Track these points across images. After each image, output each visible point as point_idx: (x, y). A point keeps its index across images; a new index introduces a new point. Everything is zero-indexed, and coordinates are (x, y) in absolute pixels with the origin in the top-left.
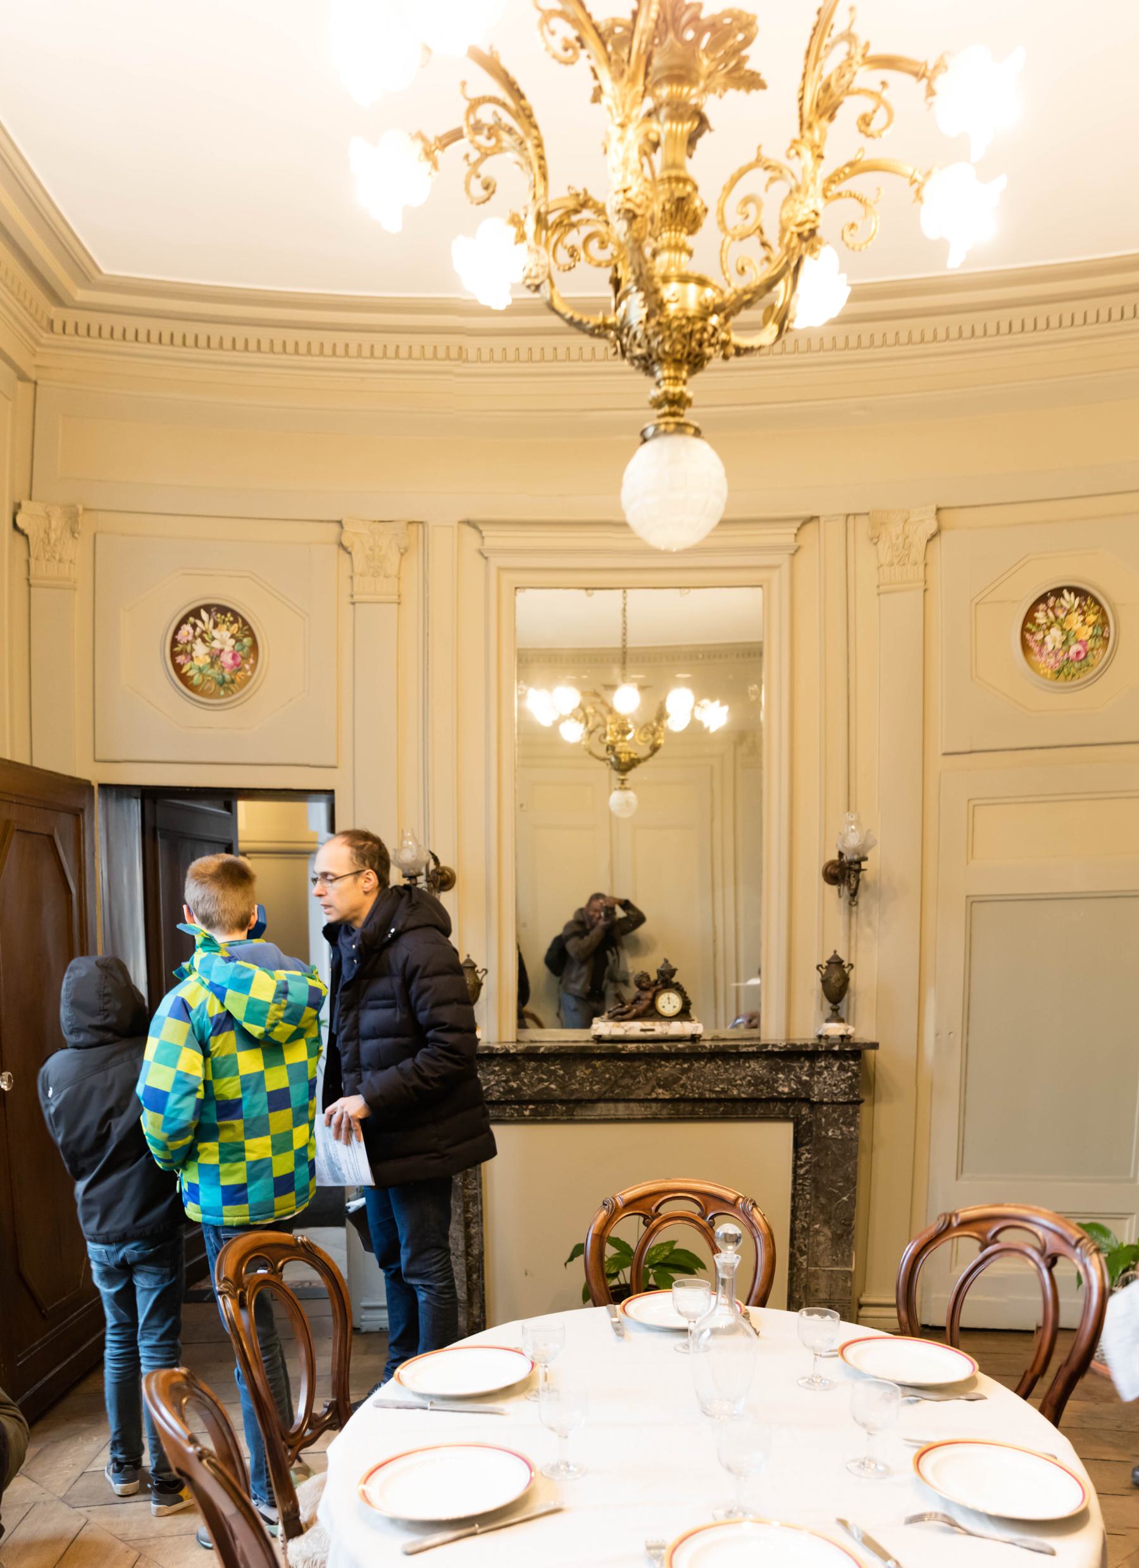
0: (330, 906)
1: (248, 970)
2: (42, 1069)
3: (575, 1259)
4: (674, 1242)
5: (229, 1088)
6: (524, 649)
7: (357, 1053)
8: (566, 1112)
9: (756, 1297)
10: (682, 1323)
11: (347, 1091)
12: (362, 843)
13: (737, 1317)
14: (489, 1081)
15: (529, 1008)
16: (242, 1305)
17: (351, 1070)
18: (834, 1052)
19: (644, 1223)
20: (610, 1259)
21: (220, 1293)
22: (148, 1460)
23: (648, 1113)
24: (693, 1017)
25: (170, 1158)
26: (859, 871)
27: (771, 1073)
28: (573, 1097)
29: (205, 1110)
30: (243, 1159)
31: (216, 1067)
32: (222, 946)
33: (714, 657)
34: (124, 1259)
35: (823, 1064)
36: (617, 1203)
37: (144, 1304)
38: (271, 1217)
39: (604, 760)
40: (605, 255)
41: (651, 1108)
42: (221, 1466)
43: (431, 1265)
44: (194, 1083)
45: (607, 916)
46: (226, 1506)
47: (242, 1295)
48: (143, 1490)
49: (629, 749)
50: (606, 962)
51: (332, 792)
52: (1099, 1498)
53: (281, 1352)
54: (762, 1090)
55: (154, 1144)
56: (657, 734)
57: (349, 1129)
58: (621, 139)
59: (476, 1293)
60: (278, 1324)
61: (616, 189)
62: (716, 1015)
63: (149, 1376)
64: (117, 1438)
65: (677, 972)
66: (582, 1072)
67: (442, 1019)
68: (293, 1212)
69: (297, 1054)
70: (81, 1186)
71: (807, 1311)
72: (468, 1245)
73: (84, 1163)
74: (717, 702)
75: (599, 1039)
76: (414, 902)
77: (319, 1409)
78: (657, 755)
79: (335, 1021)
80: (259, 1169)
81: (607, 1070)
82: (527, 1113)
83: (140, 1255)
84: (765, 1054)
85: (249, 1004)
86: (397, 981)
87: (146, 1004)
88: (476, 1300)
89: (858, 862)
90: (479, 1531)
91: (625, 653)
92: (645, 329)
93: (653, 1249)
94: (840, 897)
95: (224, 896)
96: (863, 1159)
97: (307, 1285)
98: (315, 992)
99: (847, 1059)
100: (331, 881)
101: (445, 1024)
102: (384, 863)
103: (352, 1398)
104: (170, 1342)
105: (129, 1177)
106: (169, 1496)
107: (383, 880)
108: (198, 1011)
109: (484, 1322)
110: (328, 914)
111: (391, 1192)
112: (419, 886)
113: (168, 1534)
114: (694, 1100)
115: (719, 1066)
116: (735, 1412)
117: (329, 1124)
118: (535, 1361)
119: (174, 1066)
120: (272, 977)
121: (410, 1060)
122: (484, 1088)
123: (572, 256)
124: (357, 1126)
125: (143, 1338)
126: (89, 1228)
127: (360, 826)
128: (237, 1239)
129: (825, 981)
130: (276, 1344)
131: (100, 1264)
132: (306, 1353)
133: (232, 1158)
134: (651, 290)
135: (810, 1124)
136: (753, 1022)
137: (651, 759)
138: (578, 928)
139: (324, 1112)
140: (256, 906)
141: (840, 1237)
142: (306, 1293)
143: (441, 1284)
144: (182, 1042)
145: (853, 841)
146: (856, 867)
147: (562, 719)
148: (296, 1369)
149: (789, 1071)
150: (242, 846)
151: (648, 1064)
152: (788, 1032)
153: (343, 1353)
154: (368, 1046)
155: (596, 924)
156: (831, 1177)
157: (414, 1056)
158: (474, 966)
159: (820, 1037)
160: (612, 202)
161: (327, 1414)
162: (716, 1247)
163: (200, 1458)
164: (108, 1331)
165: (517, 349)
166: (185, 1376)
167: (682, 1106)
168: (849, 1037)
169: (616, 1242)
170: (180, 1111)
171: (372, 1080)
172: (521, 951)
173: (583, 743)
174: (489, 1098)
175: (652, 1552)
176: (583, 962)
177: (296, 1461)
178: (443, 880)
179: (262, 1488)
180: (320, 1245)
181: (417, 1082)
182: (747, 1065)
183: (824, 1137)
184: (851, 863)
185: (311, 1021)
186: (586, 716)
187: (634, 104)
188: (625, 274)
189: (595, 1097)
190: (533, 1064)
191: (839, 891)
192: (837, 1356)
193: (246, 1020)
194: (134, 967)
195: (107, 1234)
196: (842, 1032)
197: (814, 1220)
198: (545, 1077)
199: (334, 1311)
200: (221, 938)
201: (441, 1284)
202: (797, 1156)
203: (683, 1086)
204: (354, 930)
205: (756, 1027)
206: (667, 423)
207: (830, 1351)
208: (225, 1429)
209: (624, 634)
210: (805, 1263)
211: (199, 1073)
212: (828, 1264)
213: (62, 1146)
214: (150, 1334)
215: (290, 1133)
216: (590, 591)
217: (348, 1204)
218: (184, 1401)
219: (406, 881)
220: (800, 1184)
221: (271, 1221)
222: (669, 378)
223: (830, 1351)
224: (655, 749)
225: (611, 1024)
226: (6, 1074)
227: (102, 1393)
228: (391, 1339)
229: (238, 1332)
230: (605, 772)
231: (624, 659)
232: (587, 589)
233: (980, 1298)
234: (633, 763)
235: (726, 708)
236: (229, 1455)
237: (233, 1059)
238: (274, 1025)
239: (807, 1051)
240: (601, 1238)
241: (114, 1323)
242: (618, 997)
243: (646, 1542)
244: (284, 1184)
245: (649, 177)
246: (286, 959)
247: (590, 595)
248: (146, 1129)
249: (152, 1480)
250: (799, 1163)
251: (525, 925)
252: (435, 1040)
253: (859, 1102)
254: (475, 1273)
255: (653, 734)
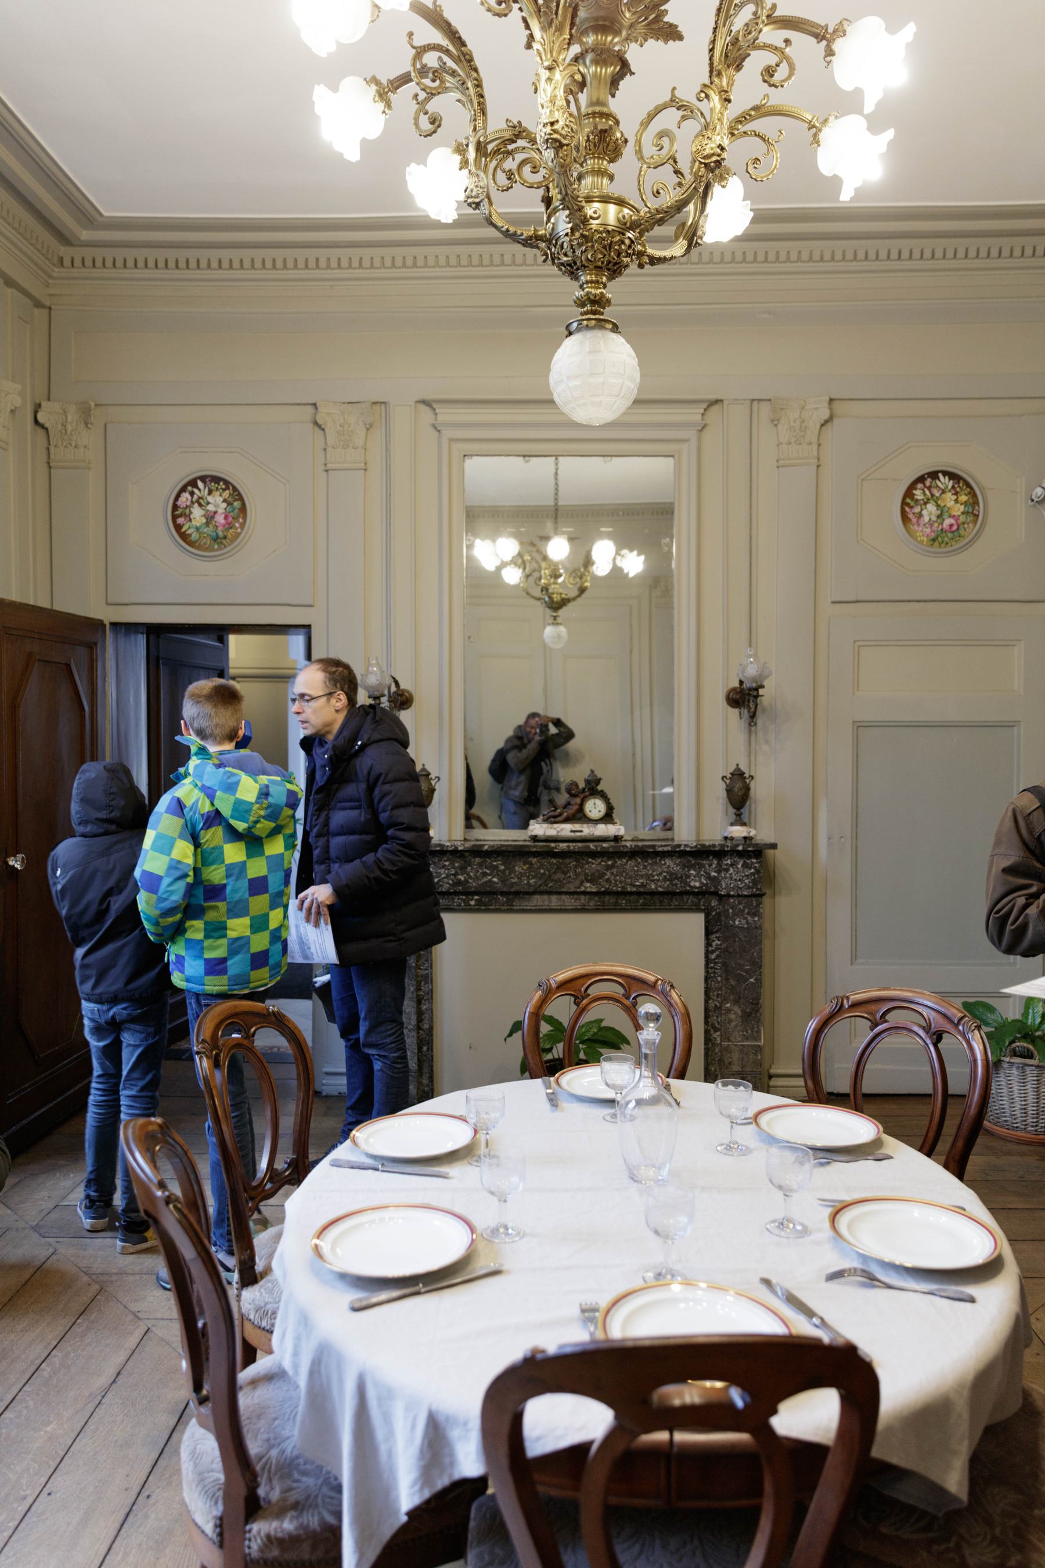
0: (306, 722)
1: (235, 775)
2: (53, 853)
3: (514, 1035)
4: (601, 1020)
5: (215, 875)
6: (471, 507)
7: (327, 848)
8: (507, 902)
9: (676, 1070)
10: (610, 1094)
11: (318, 880)
12: (334, 669)
13: (659, 1089)
14: (440, 874)
15: (474, 811)
16: (216, 1064)
17: (321, 862)
18: (738, 851)
19: (575, 1002)
20: (544, 1036)
21: (198, 1053)
22: (118, 1200)
23: (577, 904)
24: (616, 820)
25: (161, 932)
26: (757, 696)
27: (684, 869)
28: (513, 890)
29: (193, 892)
30: (225, 936)
31: (205, 856)
32: (213, 755)
33: (633, 514)
34: (113, 1017)
35: (729, 862)
36: (550, 985)
37: (129, 1058)
38: (247, 988)
39: (539, 599)
40: (538, 178)
41: (580, 900)
42: (186, 1211)
43: (386, 1037)
44: (186, 870)
45: (542, 731)
46: (187, 1251)
47: (217, 1055)
48: (111, 1228)
49: (561, 590)
50: (541, 773)
51: (309, 626)
52: (1011, 1245)
53: (249, 1109)
54: (676, 885)
55: (147, 920)
56: (584, 578)
57: (318, 913)
58: (549, 79)
59: (426, 1064)
60: (248, 1084)
61: (545, 122)
62: (635, 819)
63: (128, 1123)
64: (92, 1177)
65: (602, 782)
66: (520, 868)
67: (400, 820)
68: (266, 985)
69: (276, 847)
70: (80, 952)
71: (723, 1082)
72: (420, 1020)
73: (83, 933)
74: (635, 553)
75: (535, 838)
76: (377, 719)
77: (280, 1165)
78: (583, 596)
79: (309, 820)
80: (238, 945)
81: (542, 866)
82: (472, 903)
83: (128, 1014)
84: (679, 853)
85: (235, 803)
86: (363, 786)
87: (147, 802)
88: (425, 1070)
89: (757, 689)
90: (423, 1290)
91: (557, 510)
92: (571, 240)
93: (583, 1026)
94: (741, 718)
95: (216, 713)
96: (766, 945)
97: (276, 1050)
98: (292, 794)
99: (749, 857)
100: (308, 701)
101: (403, 824)
102: (352, 686)
103: (310, 1156)
104: (150, 1094)
105: (124, 947)
106: (135, 1236)
107: (352, 700)
108: (191, 809)
109: (432, 1090)
110: (304, 728)
111: (353, 970)
112: (382, 705)
113: (130, 1271)
114: (617, 894)
115: (639, 864)
116: (660, 1178)
117: (301, 908)
118: (478, 1128)
119: (169, 855)
120: (256, 782)
121: (373, 854)
122: (436, 880)
123: (509, 179)
124: (325, 910)
125: (125, 1089)
126: (85, 988)
127: (333, 655)
128: (215, 1006)
129: (729, 791)
130: (244, 1102)
131: (92, 1020)
132: (272, 1112)
133: (216, 934)
134: (576, 207)
135: (719, 914)
136: (668, 824)
137: (579, 599)
138: (517, 742)
139: (297, 898)
140: (243, 722)
141: (749, 1014)
142: (275, 1057)
143: (395, 1055)
144: (176, 835)
145: (752, 671)
146: (755, 693)
147: (504, 565)
148: (262, 1126)
149: (699, 868)
150: (232, 672)
151: (577, 861)
152: (698, 833)
153: (305, 1114)
154: (337, 842)
155: (533, 739)
156: (739, 961)
157: (376, 851)
158: (429, 774)
159: (726, 838)
160: (541, 133)
161: (287, 1170)
162: (639, 1024)
163: (167, 1203)
164: (94, 1080)
165: (470, 256)
166: (160, 1126)
167: (607, 898)
168: (751, 838)
169: (550, 1020)
170: (172, 892)
171: (340, 871)
172: (469, 761)
173: (522, 585)
174: (440, 889)
175: (587, 1314)
176: (522, 772)
177: (256, 1212)
178: (403, 700)
179: (222, 1236)
180: (290, 1015)
181: (378, 873)
182: (663, 862)
183: (732, 926)
184: (750, 689)
185: (288, 819)
186: (524, 562)
187: (561, 49)
188: (554, 193)
189: (532, 889)
190: (478, 860)
191: (740, 713)
192: (751, 1123)
193: (232, 817)
194: (137, 771)
195: (100, 994)
196: (745, 834)
197: (725, 1000)
198: (488, 871)
199: (299, 1075)
200: (213, 749)
201: (395, 1055)
202: (708, 943)
203: (608, 881)
204: (326, 743)
205: (670, 829)
206: (588, 319)
207: (745, 1119)
208: (192, 1177)
209: (556, 494)
210: (718, 1039)
211: (190, 861)
212: (739, 1039)
213: (65, 918)
214: (132, 1085)
215: (267, 915)
216: (527, 458)
217: (315, 980)
218: (157, 1148)
219: (371, 701)
220: (712, 968)
221: (246, 991)
222: (591, 282)
223: (745, 1119)
224: (582, 590)
225: (545, 825)
226: (20, 856)
227: (83, 1134)
228: (349, 1103)
229: (211, 1090)
230: (539, 610)
231: (556, 515)
232: (524, 456)
233: (879, 1066)
234: (564, 602)
235: (642, 558)
236: (194, 1201)
237: (219, 850)
238: (256, 822)
239: (715, 851)
240: (537, 1015)
241: (100, 1072)
242: (551, 802)
243: (581, 1305)
244: (259, 960)
245: (575, 113)
246: (268, 766)
247: (527, 462)
248: (141, 906)
249: (121, 1219)
250: (710, 949)
251: (472, 740)
252: (394, 838)
253: (761, 895)
254: (424, 1045)
255: (581, 578)
